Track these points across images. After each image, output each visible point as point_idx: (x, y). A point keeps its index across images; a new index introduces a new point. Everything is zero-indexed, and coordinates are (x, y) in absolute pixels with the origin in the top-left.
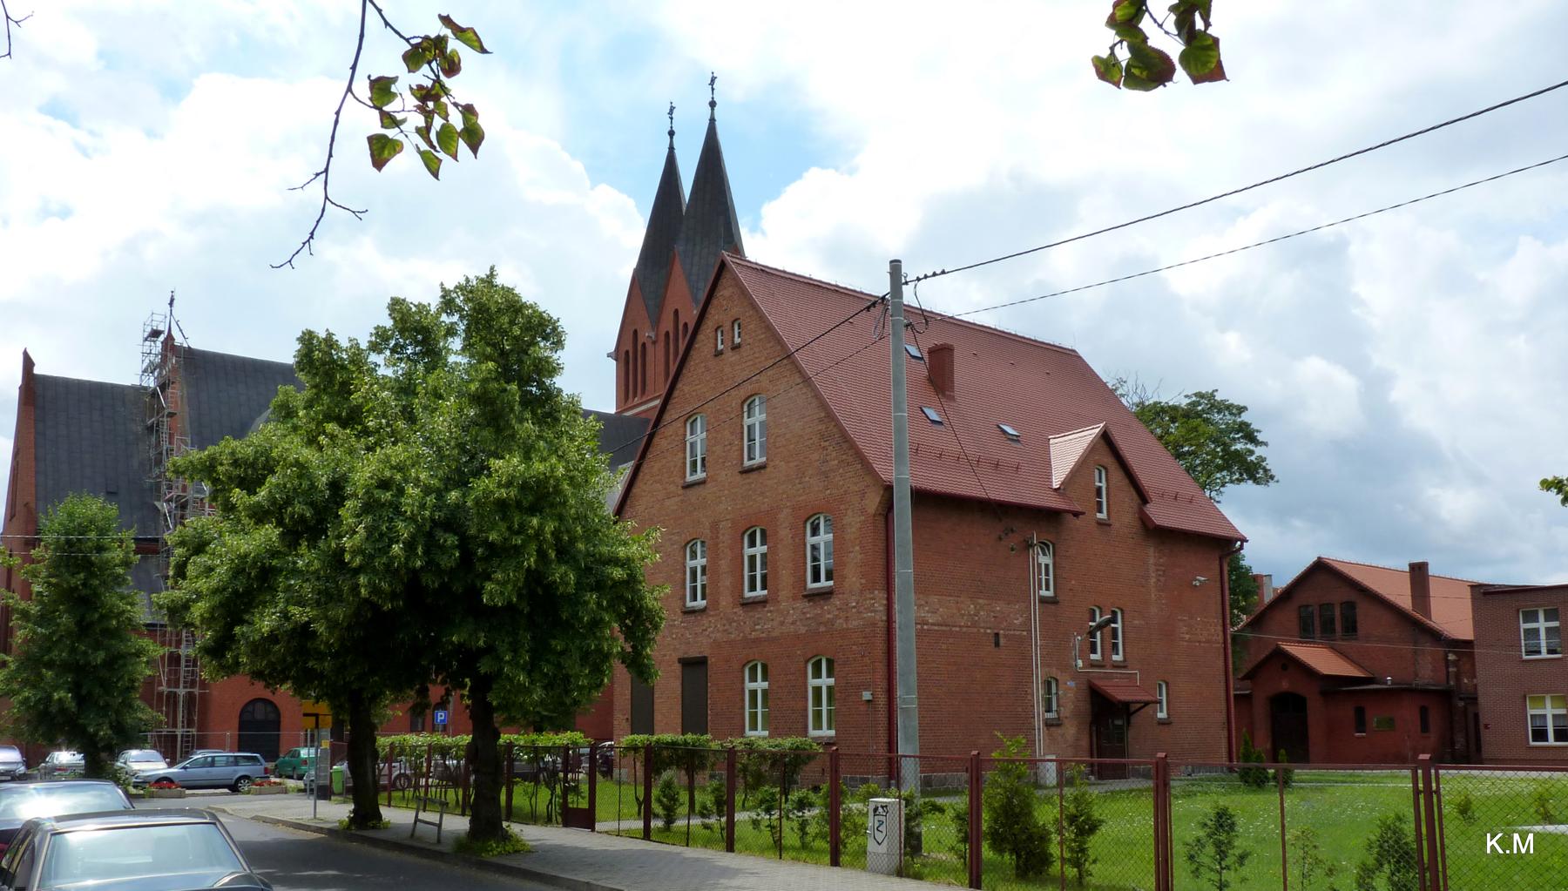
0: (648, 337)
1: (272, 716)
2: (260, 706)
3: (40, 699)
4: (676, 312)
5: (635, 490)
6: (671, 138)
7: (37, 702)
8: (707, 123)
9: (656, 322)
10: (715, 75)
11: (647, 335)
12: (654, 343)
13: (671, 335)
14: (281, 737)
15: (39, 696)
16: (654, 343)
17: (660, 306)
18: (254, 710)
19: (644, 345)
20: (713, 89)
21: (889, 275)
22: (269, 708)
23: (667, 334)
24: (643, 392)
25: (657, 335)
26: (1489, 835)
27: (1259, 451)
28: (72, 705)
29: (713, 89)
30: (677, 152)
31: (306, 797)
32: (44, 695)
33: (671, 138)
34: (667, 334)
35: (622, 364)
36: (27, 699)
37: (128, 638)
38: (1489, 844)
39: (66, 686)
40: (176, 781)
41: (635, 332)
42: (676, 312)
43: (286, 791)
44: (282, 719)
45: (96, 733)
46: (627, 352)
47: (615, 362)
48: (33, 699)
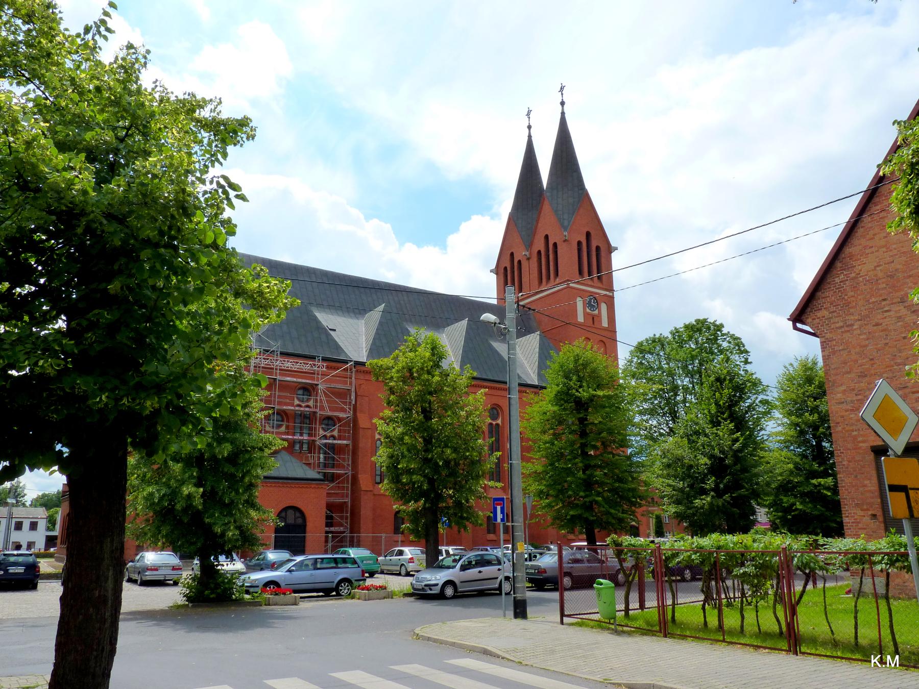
0: (525, 255)
1: (300, 521)
2: (291, 512)
3: (164, 495)
4: (547, 237)
5: (847, 250)
6: (530, 130)
7: (161, 499)
8: (527, 138)
9: (529, 245)
10: (563, 85)
11: (524, 253)
12: (528, 259)
13: (509, 269)
14: (307, 539)
15: (163, 492)
16: (528, 259)
17: (533, 233)
18: (286, 515)
19: (519, 262)
20: (562, 94)
21: (613, 244)
22: (298, 514)
23: (539, 252)
24: (557, 274)
25: (530, 254)
26: (872, 656)
27: (754, 377)
28: (198, 502)
29: (562, 94)
30: (566, 116)
31: (501, 612)
32: (169, 491)
33: (530, 130)
34: (539, 252)
35: (502, 277)
36: (151, 494)
37: (250, 432)
38: (873, 661)
39: (193, 481)
40: (282, 585)
41: (512, 254)
42: (547, 237)
43: (390, 595)
44: (308, 524)
45: (223, 534)
46: (506, 268)
47: (495, 276)
48: (157, 495)
